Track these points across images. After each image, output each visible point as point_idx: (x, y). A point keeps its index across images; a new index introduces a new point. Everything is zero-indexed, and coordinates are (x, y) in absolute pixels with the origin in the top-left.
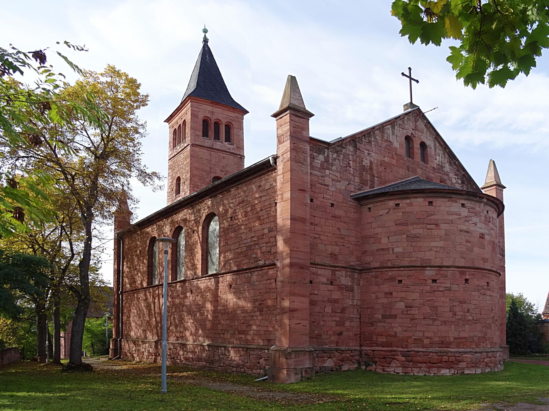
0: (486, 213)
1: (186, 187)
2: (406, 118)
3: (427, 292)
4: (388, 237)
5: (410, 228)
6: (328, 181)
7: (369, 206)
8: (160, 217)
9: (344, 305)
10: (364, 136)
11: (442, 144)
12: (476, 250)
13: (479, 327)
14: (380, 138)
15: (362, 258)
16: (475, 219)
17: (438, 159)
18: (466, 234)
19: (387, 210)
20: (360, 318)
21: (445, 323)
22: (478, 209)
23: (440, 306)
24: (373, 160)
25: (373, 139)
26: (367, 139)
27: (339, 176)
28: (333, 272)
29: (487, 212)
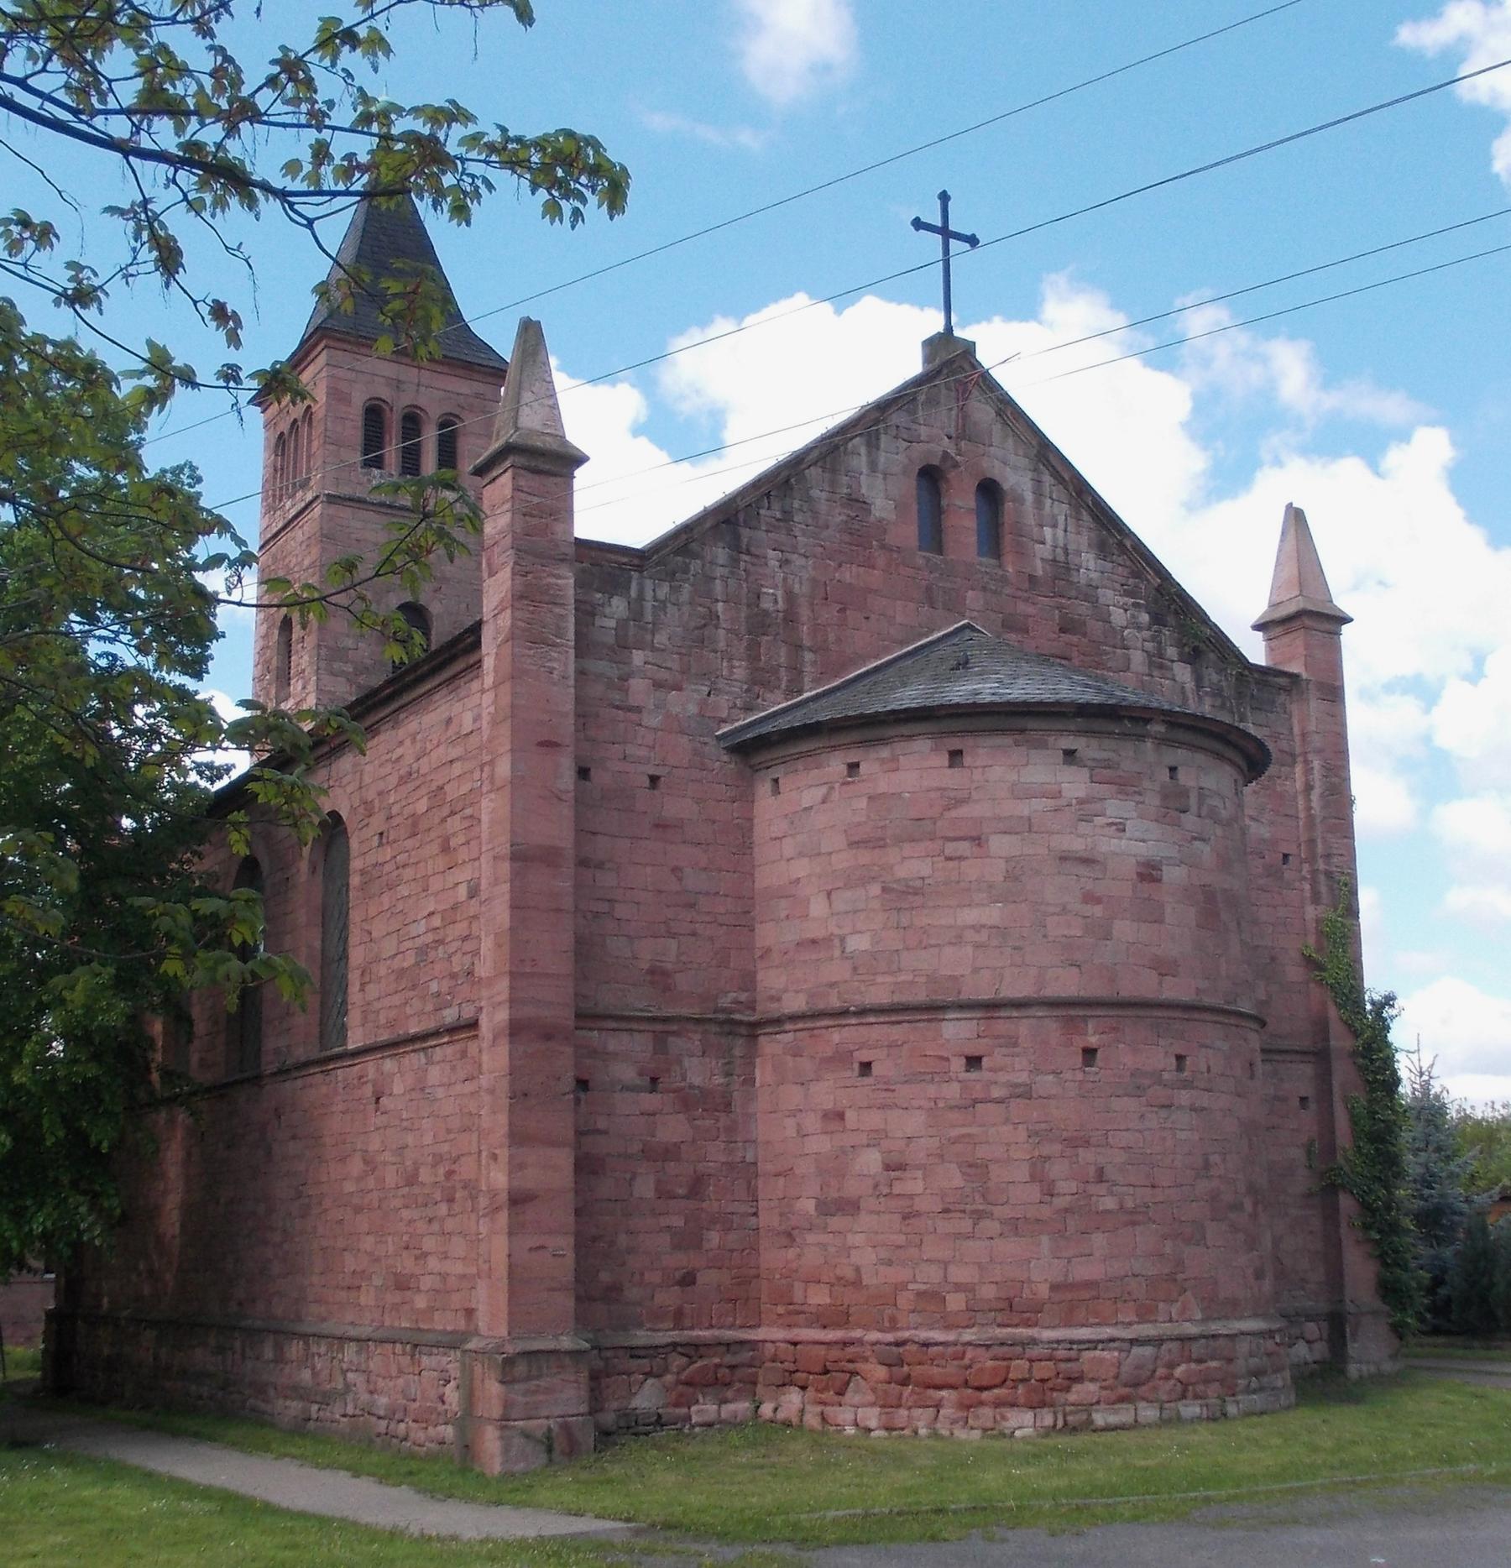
4: (829, 894)
5: (892, 855)
9: (700, 1167)
18: (1082, 870)
25: (796, 504)
26: (776, 506)
28: (660, 1040)
29: (1173, 770)
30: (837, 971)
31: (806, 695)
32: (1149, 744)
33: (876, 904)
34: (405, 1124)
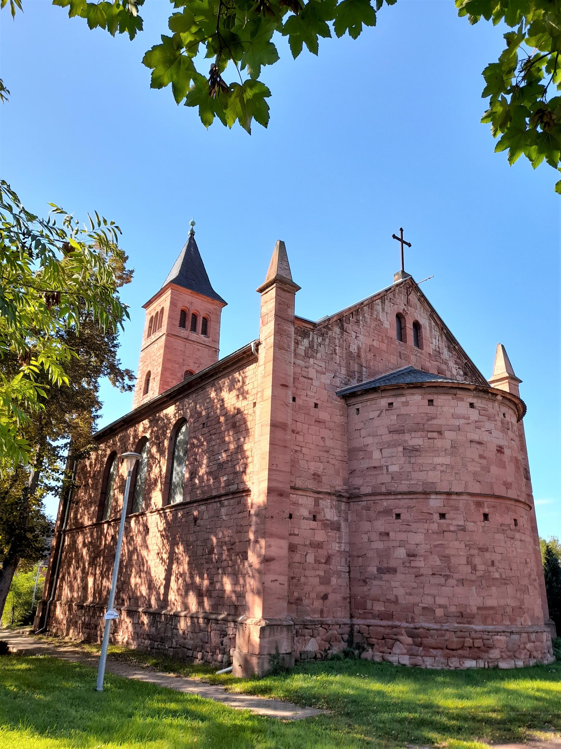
0: (503, 417)
1: (155, 384)
2: (397, 291)
3: (433, 533)
4: (381, 450)
5: (407, 436)
6: (312, 373)
7: (357, 406)
8: (123, 425)
10: (352, 313)
11: (439, 323)
12: (494, 469)
13: (510, 590)
14: (369, 317)
15: (350, 480)
16: (489, 425)
17: (434, 343)
18: (478, 446)
19: (379, 412)
20: (349, 572)
21: (462, 582)
22: (491, 410)
23: (454, 555)
24: (361, 345)
25: (361, 318)
26: (355, 317)
27: (324, 366)
28: (317, 501)
29: (504, 414)
30: (386, 479)
31: (364, 382)
32: (496, 404)
33: (401, 454)
34: (208, 530)
